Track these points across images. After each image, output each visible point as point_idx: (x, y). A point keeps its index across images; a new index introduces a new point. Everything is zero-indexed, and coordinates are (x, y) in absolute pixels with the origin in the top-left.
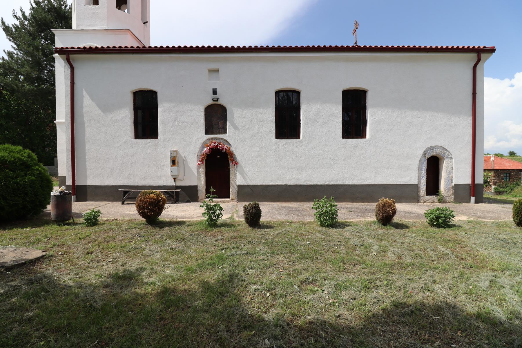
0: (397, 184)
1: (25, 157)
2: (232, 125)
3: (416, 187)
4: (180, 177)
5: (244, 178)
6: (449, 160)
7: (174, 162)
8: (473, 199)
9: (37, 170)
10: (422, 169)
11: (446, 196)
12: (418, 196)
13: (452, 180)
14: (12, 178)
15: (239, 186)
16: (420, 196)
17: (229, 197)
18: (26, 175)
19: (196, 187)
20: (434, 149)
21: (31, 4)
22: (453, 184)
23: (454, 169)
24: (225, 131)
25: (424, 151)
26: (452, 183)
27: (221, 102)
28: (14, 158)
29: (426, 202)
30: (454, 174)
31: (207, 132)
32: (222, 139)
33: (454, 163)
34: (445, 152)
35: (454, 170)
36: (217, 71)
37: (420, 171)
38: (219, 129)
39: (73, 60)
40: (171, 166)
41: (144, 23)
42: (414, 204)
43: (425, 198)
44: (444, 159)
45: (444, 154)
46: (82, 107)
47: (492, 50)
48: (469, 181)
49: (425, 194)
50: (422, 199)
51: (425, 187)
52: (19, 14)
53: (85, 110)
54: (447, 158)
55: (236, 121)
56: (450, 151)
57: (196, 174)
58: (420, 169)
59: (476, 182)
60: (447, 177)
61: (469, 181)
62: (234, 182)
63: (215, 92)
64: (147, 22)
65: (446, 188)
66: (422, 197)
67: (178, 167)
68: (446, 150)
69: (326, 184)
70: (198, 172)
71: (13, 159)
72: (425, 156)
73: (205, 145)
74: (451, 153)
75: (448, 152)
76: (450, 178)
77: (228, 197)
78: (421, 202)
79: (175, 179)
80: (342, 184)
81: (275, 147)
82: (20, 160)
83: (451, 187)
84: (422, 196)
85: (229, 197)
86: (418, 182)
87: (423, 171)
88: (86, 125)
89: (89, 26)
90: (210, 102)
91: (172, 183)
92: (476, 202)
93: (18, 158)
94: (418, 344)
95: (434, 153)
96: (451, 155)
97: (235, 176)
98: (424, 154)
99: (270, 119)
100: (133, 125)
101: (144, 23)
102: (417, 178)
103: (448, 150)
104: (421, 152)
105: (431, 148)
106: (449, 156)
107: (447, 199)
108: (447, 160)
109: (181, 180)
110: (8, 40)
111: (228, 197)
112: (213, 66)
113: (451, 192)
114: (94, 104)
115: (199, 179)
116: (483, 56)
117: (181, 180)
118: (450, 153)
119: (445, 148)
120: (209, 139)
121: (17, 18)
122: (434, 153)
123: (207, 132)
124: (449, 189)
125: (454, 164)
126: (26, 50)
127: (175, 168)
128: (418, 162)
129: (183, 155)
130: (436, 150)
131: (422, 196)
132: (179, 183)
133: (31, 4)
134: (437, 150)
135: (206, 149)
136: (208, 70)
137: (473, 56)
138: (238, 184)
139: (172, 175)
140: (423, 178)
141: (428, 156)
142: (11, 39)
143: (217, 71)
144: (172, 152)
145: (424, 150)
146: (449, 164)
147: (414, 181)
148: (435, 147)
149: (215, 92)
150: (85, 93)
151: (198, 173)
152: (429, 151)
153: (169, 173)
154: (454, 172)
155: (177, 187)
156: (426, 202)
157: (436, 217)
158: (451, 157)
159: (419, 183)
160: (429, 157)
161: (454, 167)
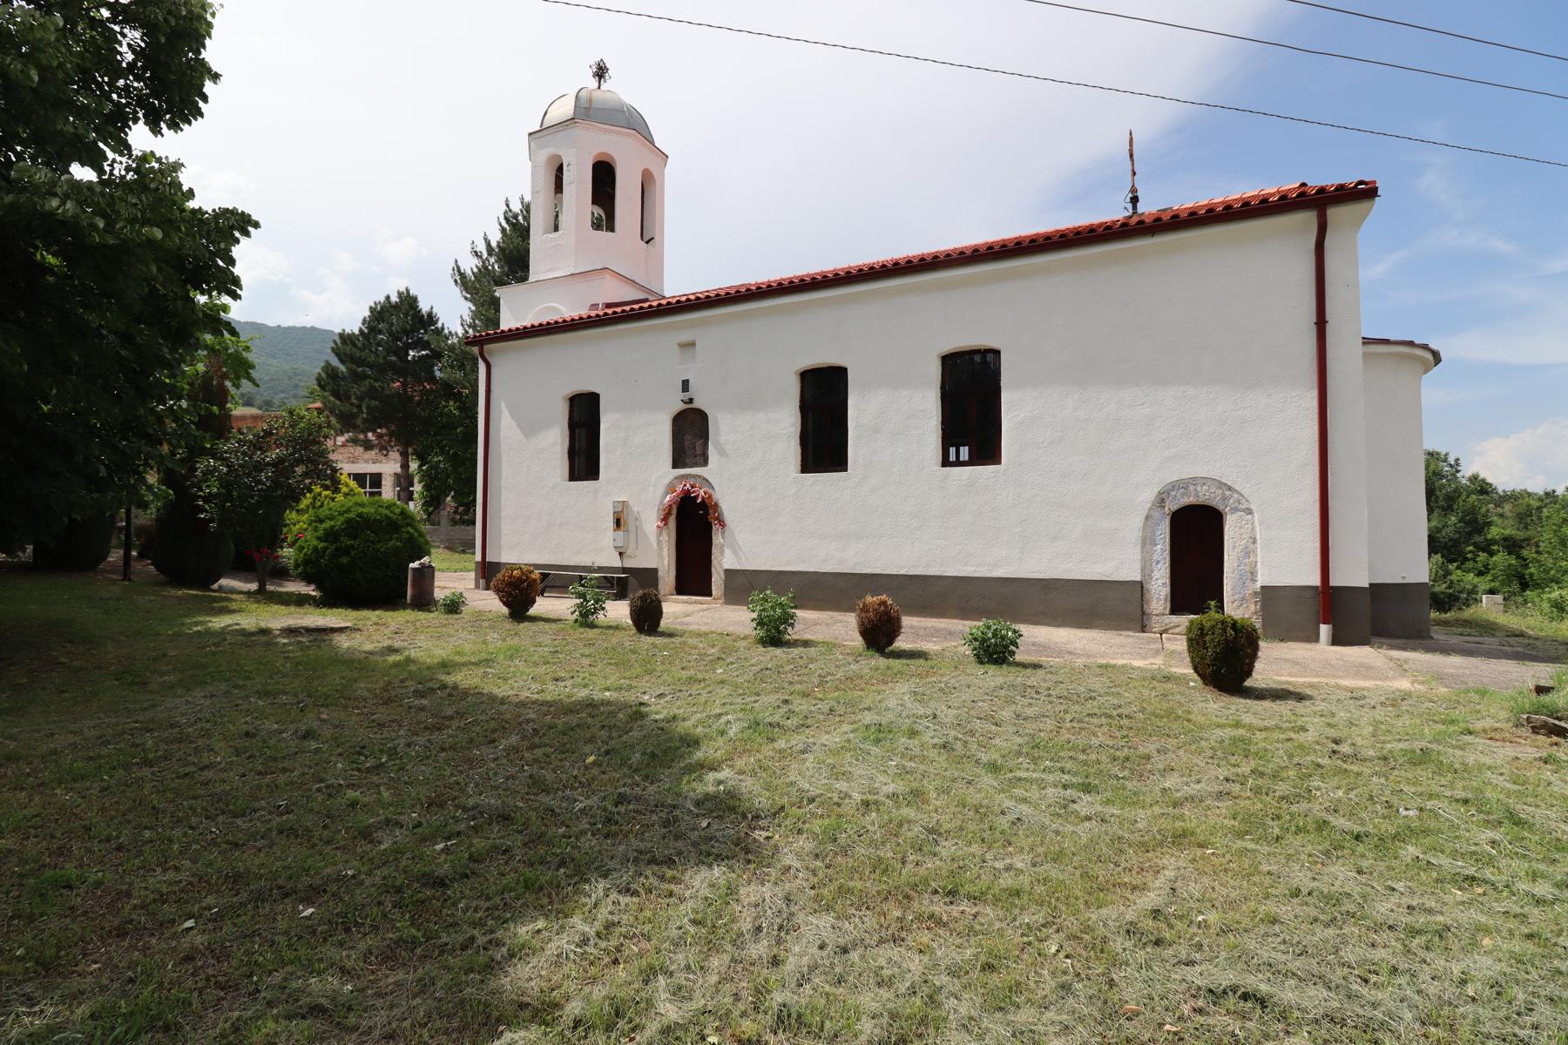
0: (1089, 578)
1: (395, 514)
2: (715, 448)
3: (1139, 589)
4: (629, 552)
5: (735, 553)
6: (1241, 517)
7: (618, 523)
8: (1325, 630)
9: (408, 532)
10: (1154, 540)
12: (1143, 613)
13: (1253, 574)
14: (373, 543)
15: (727, 572)
16: (1149, 614)
17: (710, 595)
18: (391, 539)
19: (655, 571)
20: (1192, 488)
21: (500, 225)
22: (1259, 585)
24: (704, 461)
25: (1160, 493)
26: (1254, 581)
27: (697, 404)
28: (381, 515)
31: (675, 465)
32: (699, 476)
33: (1257, 523)
34: (1228, 493)
36: (692, 344)
37: (1148, 547)
38: (696, 456)
39: (490, 352)
40: (615, 530)
41: (647, 242)
42: (1130, 633)
43: (1167, 621)
45: (1224, 498)
46: (499, 430)
47: (1365, 192)
48: (1314, 580)
49: (1165, 608)
50: (1156, 623)
51: (1166, 591)
52: (482, 248)
53: (502, 434)
54: (1235, 510)
55: (722, 440)
56: (1243, 492)
57: (655, 546)
58: (1147, 542)
59: (1333, 582)
60: (1236, 564)
61: (1314, 580)
62: (720, 564)
63: (685, 385)
64: (653, 238)
67: (627, 531)
68: (1230, 488)
69: (901, 573)
70: (659, 542)
71: (378, 517)
72: (1164, 507)
73: (671, 488)
75: (1236, 495)
76: (1248, 568)
77: (707, 592)
79: (621, 554)
80: (938, 573)
81: (794, 490)
82: (387, 517)
84: (1157, 615)
85: (710, 595)
86: (1143, 575)
87: (1159, 547)
88: (504, 459)
89: (549, 271)
90: (681, 407)
91: (617, 563)
92: (1336, 641)
93: (386, 515)
95: (1191, 499)
97: (722, 552)
98: (1161, 501)
99: (784, 432)
100: (566, 456)
101: (647, 242)
102: (1137, 566)
103: (1237, 487)
104: (1149, 495)
105: (1182, 485)
108: (1235, 516)
109: (630, 557)
110: (463, 299)
111: (707, 592)
112: (686, 337)
113: (1252, 608)
114: (514, 423)
115: (660, 556)
116: (1334, 213)
117: (630, 557)
119: (1225, 485)
120: (676, 478)
121: (477, 255)
122: (1191, 499)
123: (675, 465)
124: (1243, 599)
125: (1258, 529)
126: (484, 315)
127: (620, 533)
128: (1138, 521)
129: (635, 509)
130: (1195, 490)
131: (1157, 615)
132: (630, 563)
133: (500, 225)
134: (1199, 489)
135: (668, 498)
136: (678, 344)
137: (1306, 220)
138: (726, 566)
139: (615, 547)
140: (1159, 566)
141: (1173, 505)
143: (692, 344)
144: (616, 504)
145: (1156, 491)
146: (1241, 527)
147: (1129, 571)
148: (1194, 481)
149: (685, 385)
150: (503, 406)
151: (658, 545)
152: (1173, 493)
153: (611, 544)
155: (624, 570)
156: (1170, 631)
160: (1175, 507)
161: (1258, 537)
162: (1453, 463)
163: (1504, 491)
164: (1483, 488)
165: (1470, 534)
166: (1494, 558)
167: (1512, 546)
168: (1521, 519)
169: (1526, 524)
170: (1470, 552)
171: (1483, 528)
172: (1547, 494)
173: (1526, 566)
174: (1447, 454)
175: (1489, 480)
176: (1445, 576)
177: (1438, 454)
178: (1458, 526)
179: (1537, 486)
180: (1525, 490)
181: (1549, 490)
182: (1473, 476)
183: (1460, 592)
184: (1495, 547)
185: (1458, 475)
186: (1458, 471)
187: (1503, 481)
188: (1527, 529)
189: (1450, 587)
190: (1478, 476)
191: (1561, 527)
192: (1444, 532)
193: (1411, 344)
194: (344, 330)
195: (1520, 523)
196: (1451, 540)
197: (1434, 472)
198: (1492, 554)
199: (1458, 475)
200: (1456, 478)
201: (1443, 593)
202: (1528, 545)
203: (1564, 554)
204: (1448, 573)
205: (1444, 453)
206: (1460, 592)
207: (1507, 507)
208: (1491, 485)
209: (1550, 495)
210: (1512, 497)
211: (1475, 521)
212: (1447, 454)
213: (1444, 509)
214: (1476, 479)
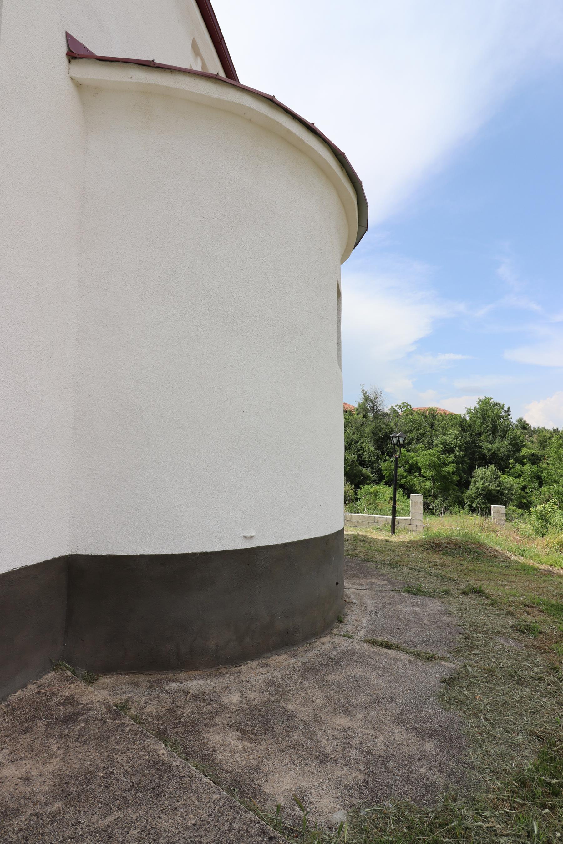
162: (507, 410)
163: (534, 428)
164: (524, 426)
165: (514, 452)
166: (525, 467)
167: (535, 459)
168: (541, 444)
169: (544, 447)
170: (512, 463)
171: (521, 448)
172: (554, 430)
173: (542, 472)
174: (503, 405)
175: (527, 422)
176: (496, 479)
177: (499, 404)
178: (508, 447)
179: (550, 427)
180: (544, 428)
181: (555, 428)
182: (520, 419)
183: (504, 489)
184: (525, 461)
185: (509, 417)
186: (509, 415)
187: (534, 423)
188: (544, 449)
189: (498, 486)
190: (522, 419)
191: (559, 449)
192: (501, 451)
193: (270, 101)
194: (558, 429)
195: (541, 446)
196: (504, 455)
197: (496, 415)
198: (523, 464)
199: (509, 417)
200: (508, 419)
201: (494, 490)
202: (544, 459)
203: (560, 465)
204: (498, 477)
205: (502, 404)
206: (504, 489)
207: (535, 437)
208: (528, 425)
209: (556, 430)
210: (538, 431)
211: (517, 444)
212: (503, 405)
213: (502, 437)
214: (521, 421)
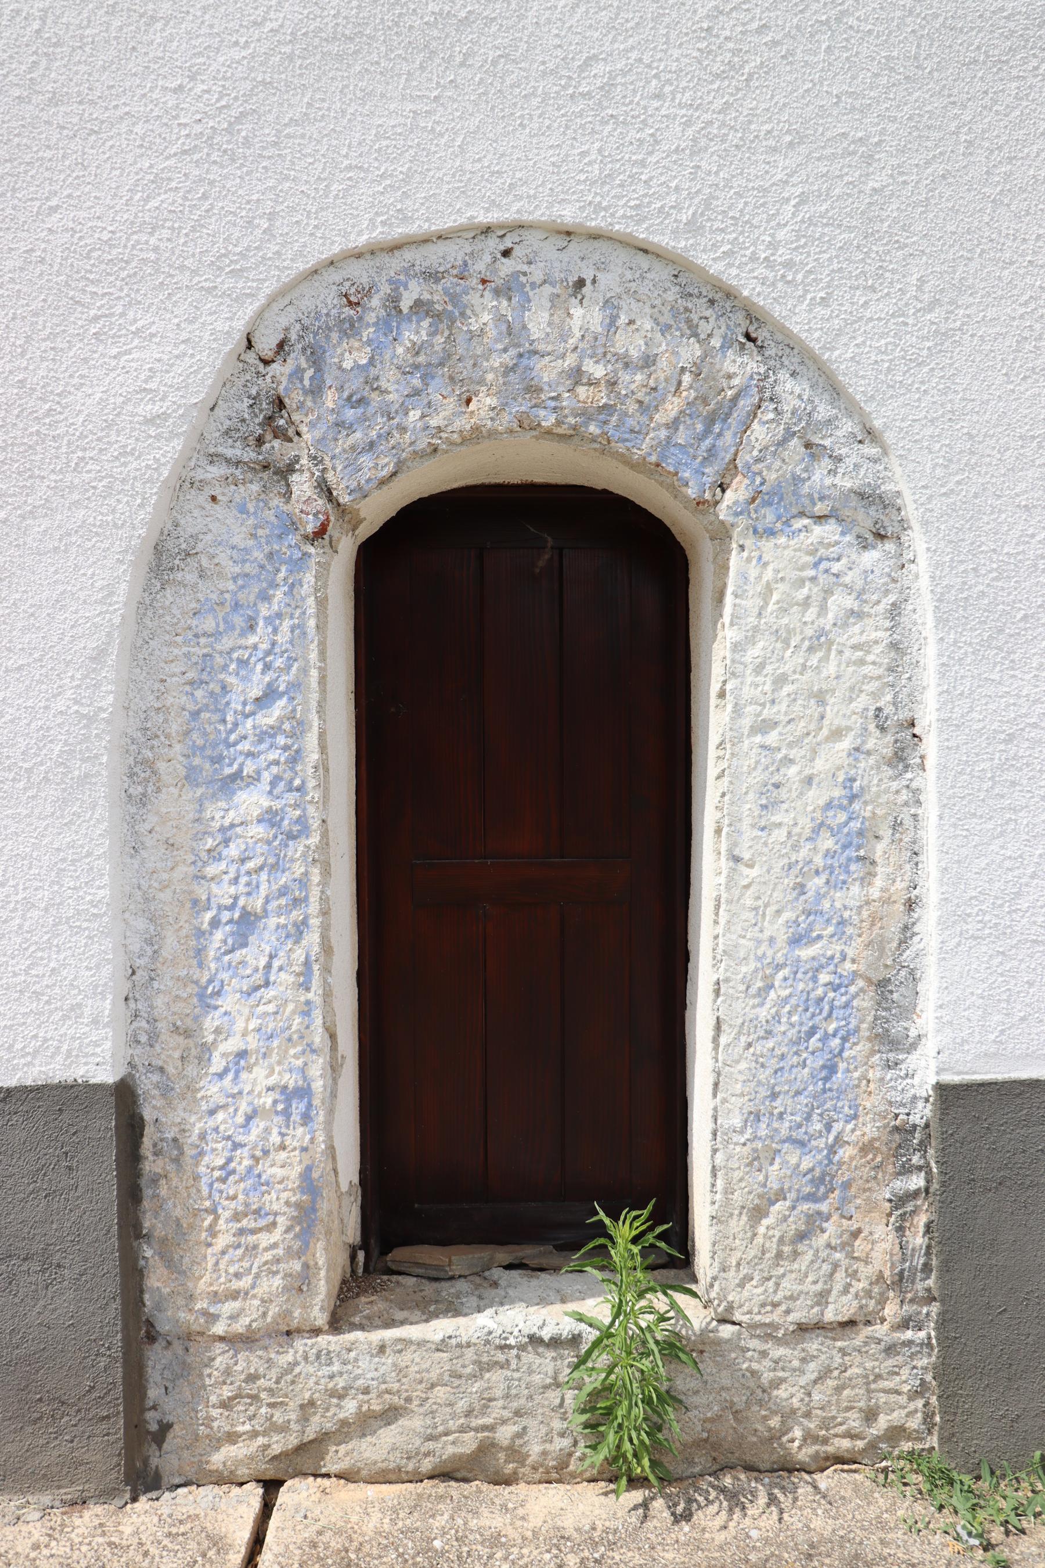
11: (768, 1332)
23: (931, 746)
29: (336, 1458)
30: (931, 861)
35: (929, 782)
44: (722, 534)
60: (778, 928)
65: (755, 1161)
66: (247, 1362)
74: (857, 388)
78: (221, 1458)
83: (870, 1129)
84: (245, 1340)
94: (5, 858)
96: (871, 434)
106: (819, 476)
107: (790, 1394)
118: (852, 409)
130: (513, 332)
142: (719, 626)
146: (820, 642)
154: (931, 810)
157: (303, 1193)
158: (866, 497)
159: (169, 1050)
161: (928, 718)
